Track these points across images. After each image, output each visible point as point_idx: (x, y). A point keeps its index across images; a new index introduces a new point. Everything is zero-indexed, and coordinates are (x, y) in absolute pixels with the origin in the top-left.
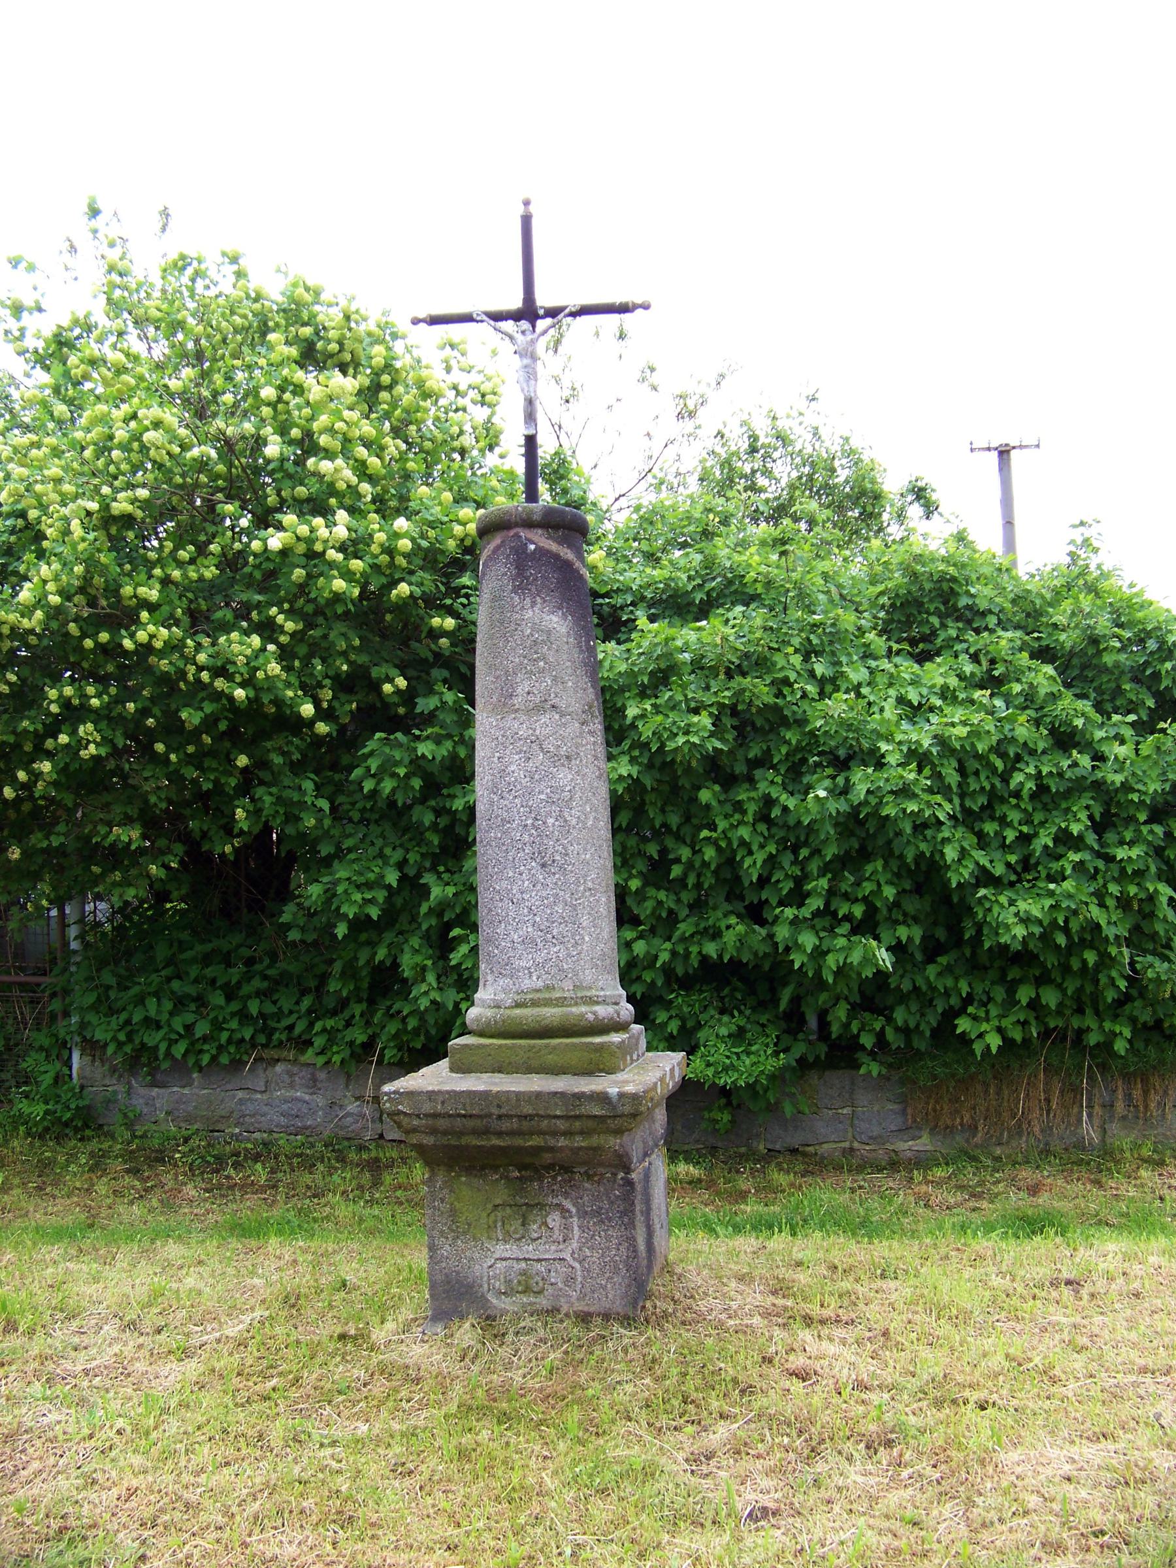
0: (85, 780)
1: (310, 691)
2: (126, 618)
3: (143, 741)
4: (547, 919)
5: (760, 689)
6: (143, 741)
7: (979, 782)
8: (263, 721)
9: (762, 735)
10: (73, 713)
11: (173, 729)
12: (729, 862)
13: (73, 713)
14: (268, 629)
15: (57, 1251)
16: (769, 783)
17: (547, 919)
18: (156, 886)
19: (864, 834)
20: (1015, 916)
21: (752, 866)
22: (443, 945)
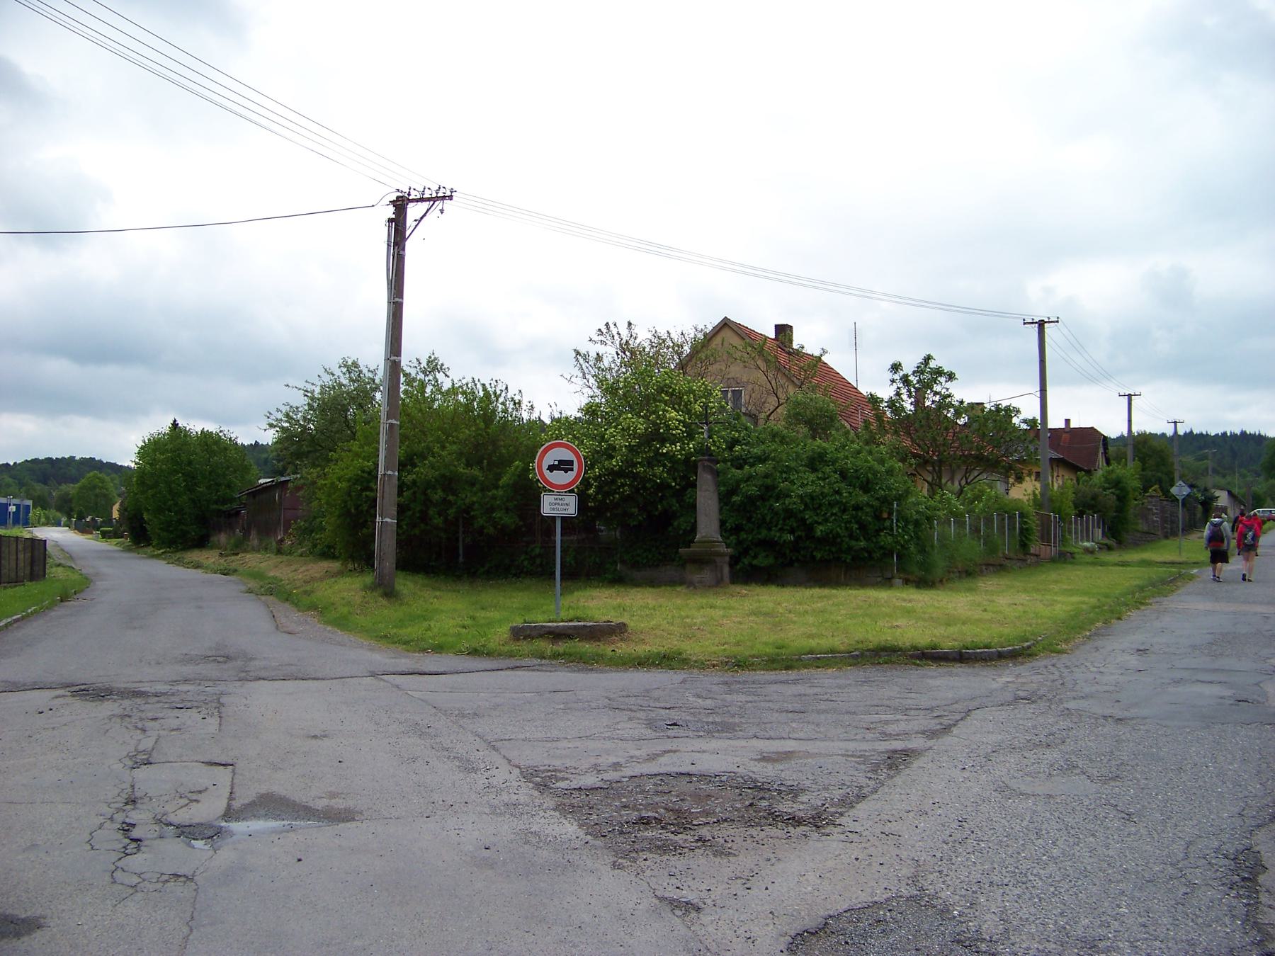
0: (626, 499)
1: (675, 480)
2: (634, 465)
3: (638, 490)
4: (708, 524)
5: (769, 481)
6: (638, 490)
7: (812, 502)
8: (664, 486)
9: (769, 491)
10: (623, 485)
11: (644, 488)
12: (764, 519)
13: (623, 485)
14: (664, 466)
15: (801, 814)
16: (772, 501)
17: (708, 524)
18: (511, 505)
19: (789, 513)
20: (819, 530)
21: (768, 519)
22: (213, 453)
